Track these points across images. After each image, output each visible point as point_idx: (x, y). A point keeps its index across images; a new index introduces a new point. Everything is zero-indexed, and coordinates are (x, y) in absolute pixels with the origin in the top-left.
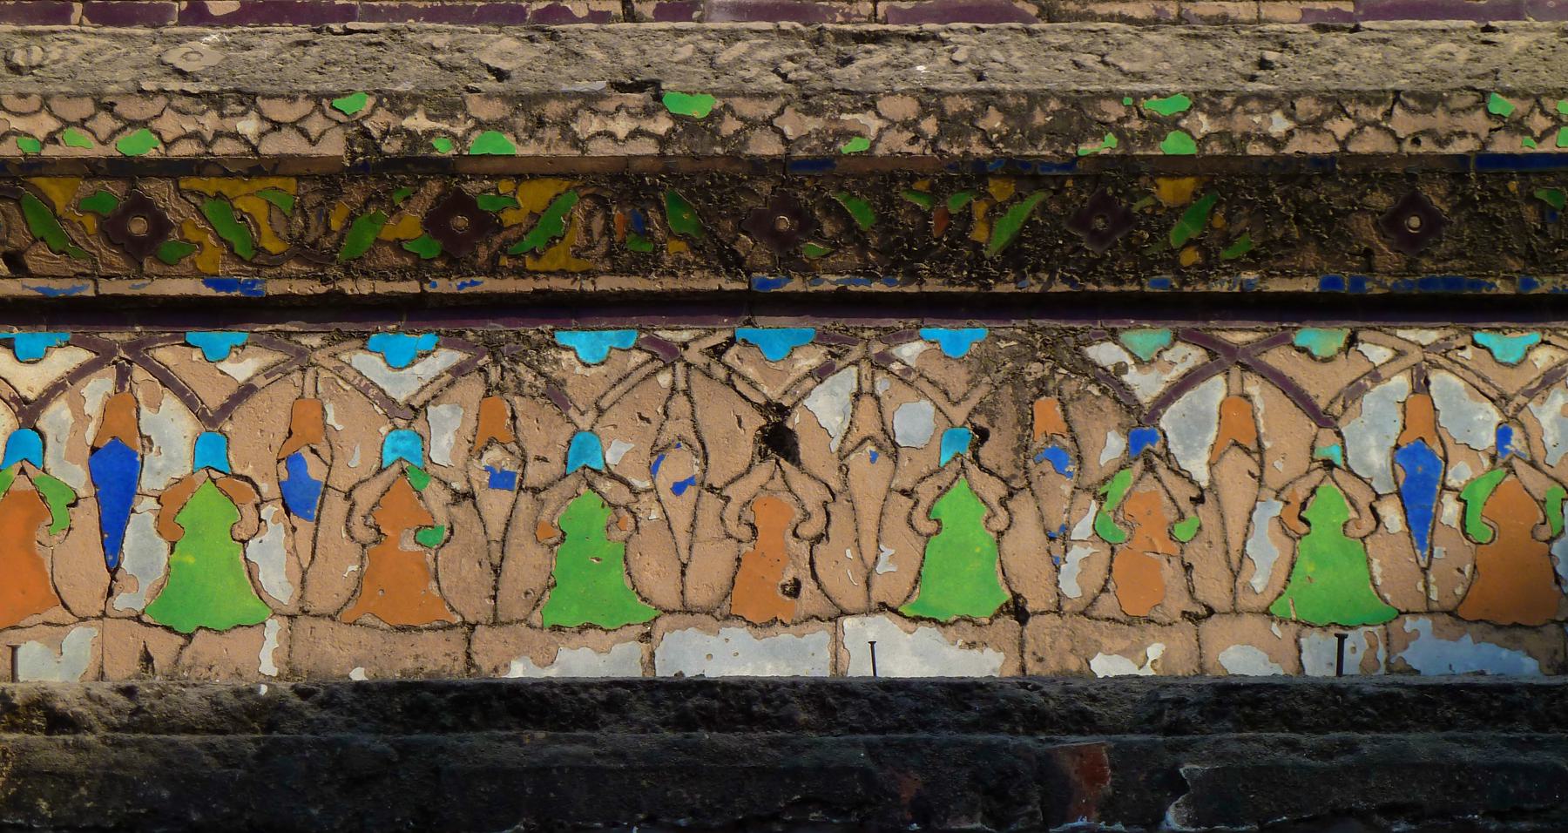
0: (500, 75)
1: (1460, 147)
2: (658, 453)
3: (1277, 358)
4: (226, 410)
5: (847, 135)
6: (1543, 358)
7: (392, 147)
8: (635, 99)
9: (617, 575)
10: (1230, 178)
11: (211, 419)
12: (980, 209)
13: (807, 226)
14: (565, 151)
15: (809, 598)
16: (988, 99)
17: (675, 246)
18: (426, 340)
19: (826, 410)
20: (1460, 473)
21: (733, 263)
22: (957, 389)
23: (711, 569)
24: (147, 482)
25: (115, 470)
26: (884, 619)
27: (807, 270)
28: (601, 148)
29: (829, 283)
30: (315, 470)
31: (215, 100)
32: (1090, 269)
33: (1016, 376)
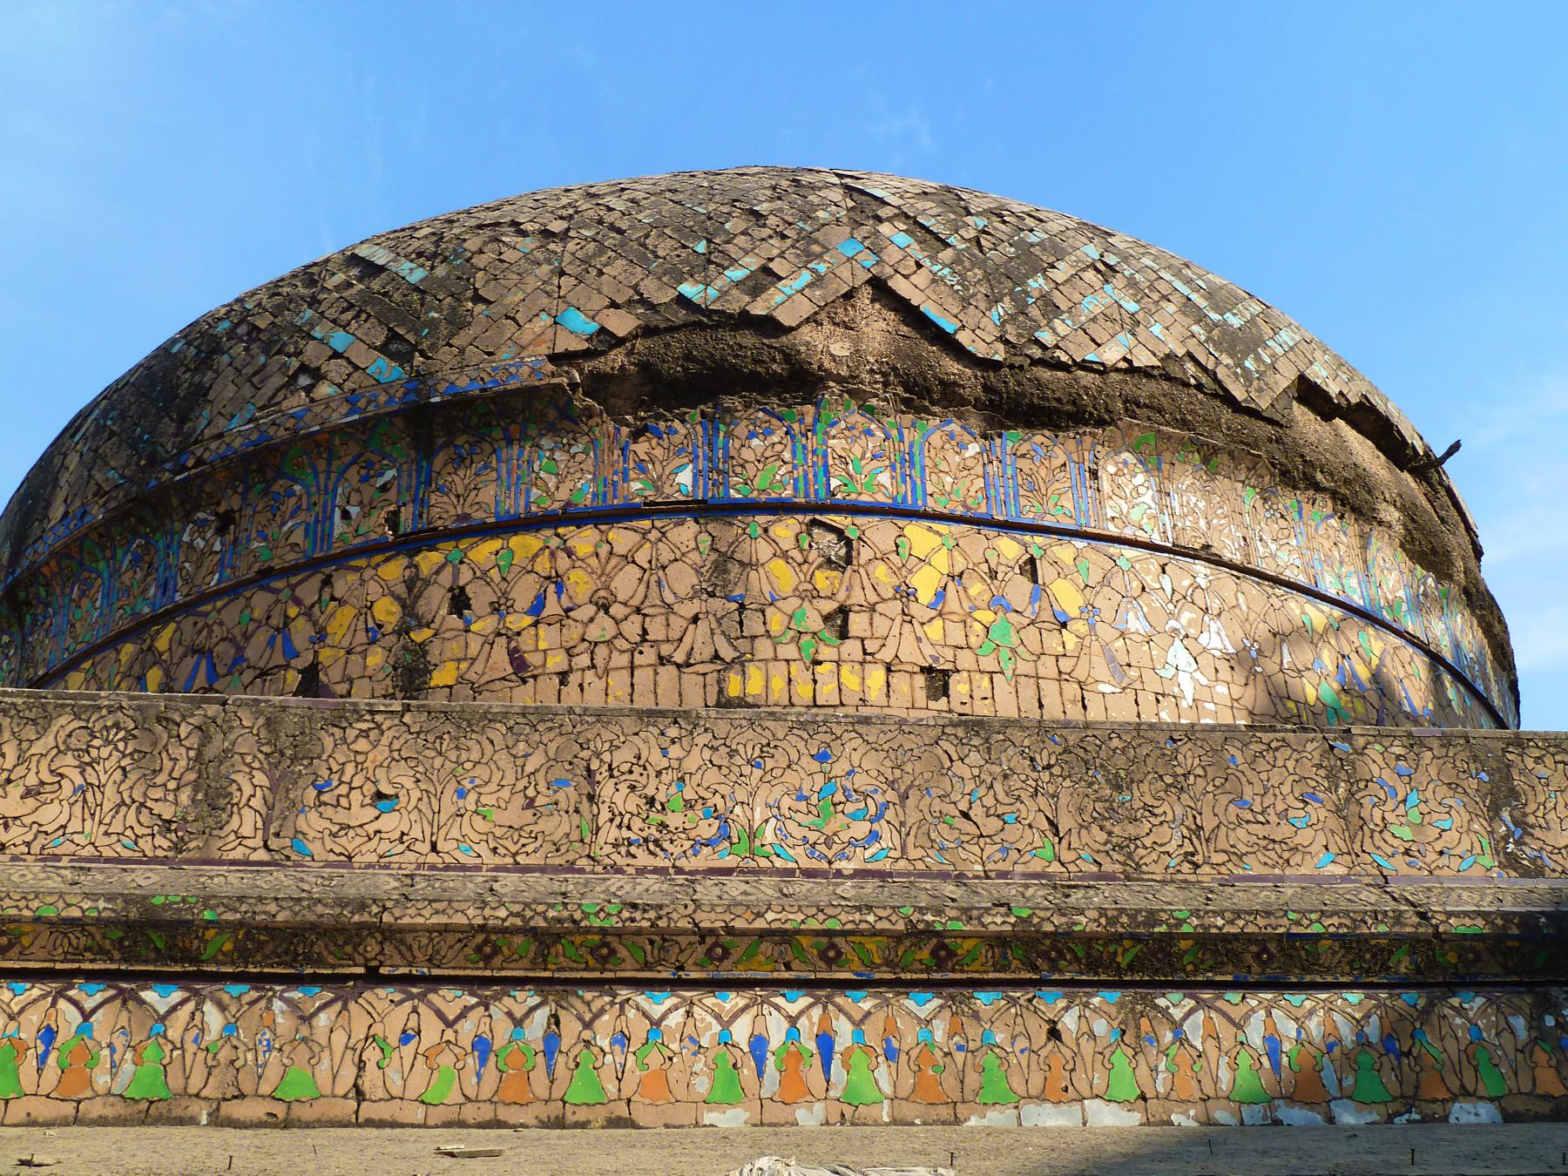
0: (953, 900)
1: (1280, 930)
2: (1014, 1038)
3: (1219, 1004)
4: (862, 1021)
5: (1076, 924)
6: (1308, 1004)
7: (921, 926)
8: (1003, 910)
9: (1004, 1084)
10: (1207, 942)
11: (857, 1024)
12: (1120, 950)
13: (1061, 956)
14: (980, 928)
15: (1071, 1093)
16: (1122, 911)
17: (1015, 962)
18: (929, 995)
19: (1069, 1022)
20: (1286, 1047)
21: (1035, 969)
22: (1114, 1015)
23: (1036, 1081)
24: (837, 1048)
25: (825, 1043)
26: (1098, 1100)
27: (1061, 971)
28: (992, 928)
29: (1068, 976)
30: (895, 1044)
31: (858, 909)
32: (1156, 972)
33: (1133, 1010)
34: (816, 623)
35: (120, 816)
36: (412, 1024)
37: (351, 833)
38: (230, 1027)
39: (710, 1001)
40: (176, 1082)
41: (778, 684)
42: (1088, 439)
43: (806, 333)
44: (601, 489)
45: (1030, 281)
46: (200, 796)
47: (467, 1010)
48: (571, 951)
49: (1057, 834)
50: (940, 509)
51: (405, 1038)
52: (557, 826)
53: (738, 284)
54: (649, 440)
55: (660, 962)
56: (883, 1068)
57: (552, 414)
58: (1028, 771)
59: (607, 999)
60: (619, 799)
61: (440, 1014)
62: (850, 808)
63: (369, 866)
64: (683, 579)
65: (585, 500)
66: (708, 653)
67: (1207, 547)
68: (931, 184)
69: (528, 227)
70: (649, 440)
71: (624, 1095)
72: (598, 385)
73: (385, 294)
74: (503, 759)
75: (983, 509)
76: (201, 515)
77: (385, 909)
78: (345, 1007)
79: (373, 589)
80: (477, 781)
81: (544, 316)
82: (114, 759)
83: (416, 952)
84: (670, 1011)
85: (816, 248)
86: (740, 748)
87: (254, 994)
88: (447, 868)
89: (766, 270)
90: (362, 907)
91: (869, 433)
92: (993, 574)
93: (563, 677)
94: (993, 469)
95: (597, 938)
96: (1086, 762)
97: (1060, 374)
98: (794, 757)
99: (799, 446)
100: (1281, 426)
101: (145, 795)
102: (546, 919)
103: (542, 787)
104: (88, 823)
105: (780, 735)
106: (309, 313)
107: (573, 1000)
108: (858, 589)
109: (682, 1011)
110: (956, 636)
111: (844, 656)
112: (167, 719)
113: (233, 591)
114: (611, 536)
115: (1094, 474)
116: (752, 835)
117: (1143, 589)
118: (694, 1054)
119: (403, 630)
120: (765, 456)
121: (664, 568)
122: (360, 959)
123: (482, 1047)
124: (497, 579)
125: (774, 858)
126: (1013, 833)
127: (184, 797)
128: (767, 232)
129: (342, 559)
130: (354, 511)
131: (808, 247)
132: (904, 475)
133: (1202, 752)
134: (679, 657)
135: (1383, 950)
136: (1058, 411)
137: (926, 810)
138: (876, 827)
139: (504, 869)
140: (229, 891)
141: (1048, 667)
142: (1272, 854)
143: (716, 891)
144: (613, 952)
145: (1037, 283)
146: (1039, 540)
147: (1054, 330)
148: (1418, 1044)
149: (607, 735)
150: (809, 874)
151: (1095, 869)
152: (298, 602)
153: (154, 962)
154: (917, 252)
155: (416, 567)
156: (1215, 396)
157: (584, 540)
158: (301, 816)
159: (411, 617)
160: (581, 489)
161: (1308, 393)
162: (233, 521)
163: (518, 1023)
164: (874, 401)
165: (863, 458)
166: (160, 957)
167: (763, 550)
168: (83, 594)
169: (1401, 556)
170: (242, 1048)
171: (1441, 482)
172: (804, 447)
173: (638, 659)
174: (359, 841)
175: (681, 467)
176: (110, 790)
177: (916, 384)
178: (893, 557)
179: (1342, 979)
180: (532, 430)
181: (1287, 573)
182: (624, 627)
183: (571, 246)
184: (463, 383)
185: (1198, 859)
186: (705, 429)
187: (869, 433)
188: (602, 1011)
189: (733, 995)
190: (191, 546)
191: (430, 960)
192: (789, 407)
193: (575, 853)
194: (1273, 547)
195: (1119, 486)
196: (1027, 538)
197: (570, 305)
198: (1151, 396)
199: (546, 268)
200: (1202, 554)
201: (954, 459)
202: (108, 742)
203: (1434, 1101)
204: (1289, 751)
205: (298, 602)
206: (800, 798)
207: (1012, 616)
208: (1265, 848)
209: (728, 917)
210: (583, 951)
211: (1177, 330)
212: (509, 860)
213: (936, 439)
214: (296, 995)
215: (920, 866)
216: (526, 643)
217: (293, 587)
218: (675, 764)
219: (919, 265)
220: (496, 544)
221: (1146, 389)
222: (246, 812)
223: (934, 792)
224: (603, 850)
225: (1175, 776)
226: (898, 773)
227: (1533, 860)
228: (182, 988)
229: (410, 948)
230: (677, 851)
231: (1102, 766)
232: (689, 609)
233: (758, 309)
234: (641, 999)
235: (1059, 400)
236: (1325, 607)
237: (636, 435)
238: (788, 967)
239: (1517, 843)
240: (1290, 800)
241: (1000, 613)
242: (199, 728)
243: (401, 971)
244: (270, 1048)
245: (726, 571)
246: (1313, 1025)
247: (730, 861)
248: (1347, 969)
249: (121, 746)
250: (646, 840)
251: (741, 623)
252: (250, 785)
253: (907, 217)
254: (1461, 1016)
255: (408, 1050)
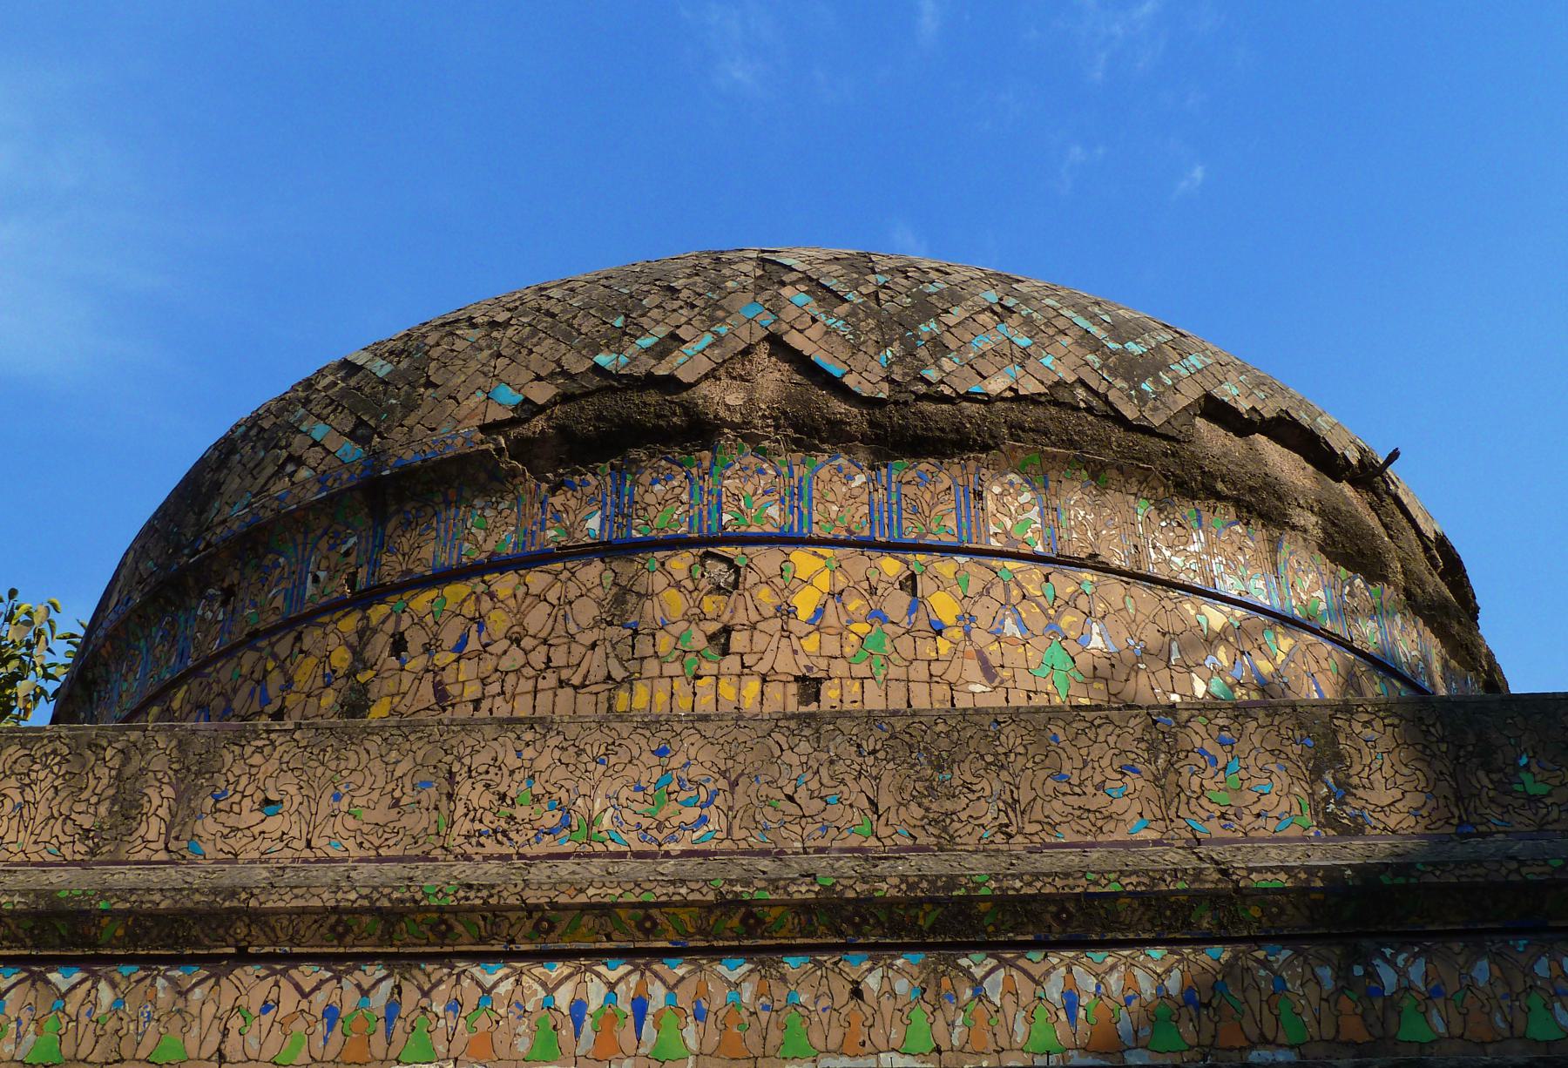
1: (1078, 890)
2: (817, 997)
3: (1021, 962)
4: (676, 985)
6: (1110, 961)
7: (729, 897)
8: (808, 880)
9: (804, 1041)
10: (1005, 903)
11: (671, 988)
18: (740, 961)
19: (872, 982)
20: (1084, 1001)
21: (840, 933)
25: (640, 1006)
27: (865, 936)
28: (797, 896)
29: (872, 940)
30: (705, 1005)
31: (673, 882)
32: (958, 934)
33: (935, 970)
34: (699, 641)
35: (48, 828)
36: (273, 996)
37: (240, 834)
38: (119, 1002)
39: (538, 970)
40: (68, 1050)
41: (661, 697)
42: (972, 464)
43: (704, 389)
44: (522, 538)
45: (922, 326)
46: (116, 808)
47: (322, 982)
48: (413, 928)
49: (876, 812)
50: (824, 535)
51: (266, 1008)
52: (416, 822)
53: (647, 350)
54: (565, 493)
55: (492, 936)
56: (692, 1027)
57: (482, 477)
58: (854, 756)
59: (446, 971)
60: (474, 796)
61: (298, 987)
62: (683, 796)
63: (253, 861)
64: (586, 611)
65: (507, 550)
66: (603, 673)
67: (1093, 556)
68: (843, 252)
69: (479, 320)
70: (565, 493)
71: (452, 1055)
72: (523, 449)
73: (359, 389)
74: (377, 766)
75: (866, 533)
76: (211, 591)
77: (252, 895)
78: (217, 983)
79: (333, 639)
80: (352, 786)
81: (479, 393)
82: (49, 780)
83: (279, 933)
84: (501, 980)
85: (720, 314)
86: (588, 748)
87: (142, 974)
88: (318, 861)
89: (673, 337)
90: (233, 893)
91: (762, 472)
92: (873, 591)
93: (477, 703)
94: (880, 495)
95: (435, 916)
96: (910, 746)
97: (944, 406)
98: (636, 752)
99: (696, 488)
100: (1178, 441)
101: (71, 809)
102: (390, 900)
103: (408, 789)
104: (22, 835)
105: (625, 735)
106: (302, 411)
107: (415, 972)
108: (741, 610)
109: (512, 980)
110: (832, 646)
111: (724, 670)
112: (96, 745)
113: (229, 653)
114: (528, 579)
115: (979, 496)
116: (591, 823)
117: (1024, 597)
118: (519, 1018)
119: (351, 674)
120: (666, 498)
121: (570, 603)
122: (231, 941)
123: (331, 1014)
124: (431, 623)
125: (609, 843)
126: (834, 812)
127: (103, 810)
128: (680, 303)
129: (310, 618)
130: (322, 575)
131: (713, 313)
132: (792, 508)
133: (1024, 732)
134: (576, 680)
135: (1182, 906)
136: (940, 440)
137: (753, 795)
138: (705, 812)
139: (367, 860)
140: (126, 885)
141: (919, 670)
142: (1086, 823)
143: (548, 872)
144: (450, 928)
145: (928, 328)
146: (921, 557)
147: (940, 368)
148: (1218, 996)
149: (469, 742)
150: (639, 855)
151: (910, 842)
152: (275, 657)
153: (60, 947)
154: (813, 308)
155: (368, 618)
156: (1106, 417)
157: (504, 584)
158: (199, 822)
159: (360, 661)
160: (504, 540)
161: (1215, 410)
162: (234, 594)
163: (365, 993)
164: (766, 443)
165: (755, 494)
166: (65, 943)
167: (660, 581)
168: (130, 669)
169: (1320, 558)
170: (126, 1019)
171: (1388, 492)
172: (701, 488)
173: (542, 684)
174: (245, 840)
175: (591, 514)
176: (43, 807)
177: (804, 425)
178: (778, 580)
179: (1146, 936)
180: (467, 493)
181: (1182, 576)
182: (533, 657)
183: (510, 332)
184: (408, 456)
185: (1012, 830)
186: (614, 480)
187: (762, 472)
188: (440, 981)
189: (559, 965)
190: (203, 619)
191: (291, 940)
192: (689, 454)
193: (431, 845)
194: (1168, 554)
195: (1004, 505)
196: (910, 557)
197: (501, 381)
198: (1037, 421)
199: (487, 353)
200: (1089, 562)
201: (843, 490)
202: (46, 766)
203: (1231, 1049)
204: (1111, 728)
205: (275, 657)
206: (639, 789)
207: (888, 627)
208: (1080, 817)
209: (552, 894)
210: (424, 928)
211: (1072, 359)
212: (373, 853)
213: (824, 473)
214: (177, 973)
215: (743, 845)
216: (448, 676)
217: (272, 645)
218: (527, 764)
219: (814, 320)
220: (433, 593)
221: (1032, 414)
222: (153, 820)
223: (762, 779)
224: (455, 840)
225: (996, 755)
226: (730, 763)
227: (1353, 818)
228: (82, 970)
229: (273, 929)
230: (521, 840)
231: (925, 749)
232: (588, 638)
233: (662, 370)
234: (476, 971)
235: (942, 430)
236: (1226, 608)
237: (553, 491)
238: (609, 939)
239: (1336, 803)
240: (1109, 773)
241: (877, 625)
242: (122, 751)
243: (266, 950)
244: (150, 1019)
245: (625, 602)
246: (1114, 981)
247: (568, 847)
248: (1148, 926)
249: (56, 769)
250: (495, 831)
251: (633, 647)
252: (159, 798)
253: (811, 279)
254: (1265, 968)
255: (267, 1019)
